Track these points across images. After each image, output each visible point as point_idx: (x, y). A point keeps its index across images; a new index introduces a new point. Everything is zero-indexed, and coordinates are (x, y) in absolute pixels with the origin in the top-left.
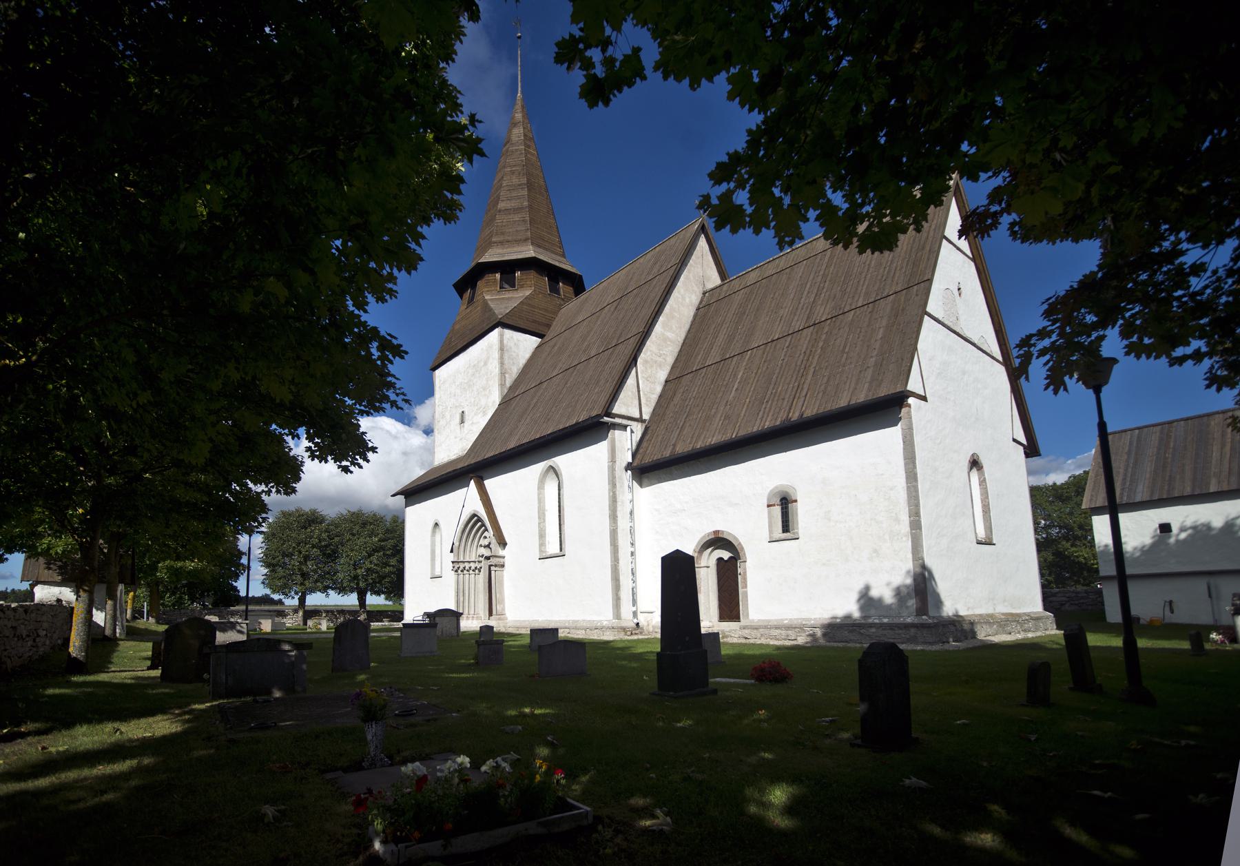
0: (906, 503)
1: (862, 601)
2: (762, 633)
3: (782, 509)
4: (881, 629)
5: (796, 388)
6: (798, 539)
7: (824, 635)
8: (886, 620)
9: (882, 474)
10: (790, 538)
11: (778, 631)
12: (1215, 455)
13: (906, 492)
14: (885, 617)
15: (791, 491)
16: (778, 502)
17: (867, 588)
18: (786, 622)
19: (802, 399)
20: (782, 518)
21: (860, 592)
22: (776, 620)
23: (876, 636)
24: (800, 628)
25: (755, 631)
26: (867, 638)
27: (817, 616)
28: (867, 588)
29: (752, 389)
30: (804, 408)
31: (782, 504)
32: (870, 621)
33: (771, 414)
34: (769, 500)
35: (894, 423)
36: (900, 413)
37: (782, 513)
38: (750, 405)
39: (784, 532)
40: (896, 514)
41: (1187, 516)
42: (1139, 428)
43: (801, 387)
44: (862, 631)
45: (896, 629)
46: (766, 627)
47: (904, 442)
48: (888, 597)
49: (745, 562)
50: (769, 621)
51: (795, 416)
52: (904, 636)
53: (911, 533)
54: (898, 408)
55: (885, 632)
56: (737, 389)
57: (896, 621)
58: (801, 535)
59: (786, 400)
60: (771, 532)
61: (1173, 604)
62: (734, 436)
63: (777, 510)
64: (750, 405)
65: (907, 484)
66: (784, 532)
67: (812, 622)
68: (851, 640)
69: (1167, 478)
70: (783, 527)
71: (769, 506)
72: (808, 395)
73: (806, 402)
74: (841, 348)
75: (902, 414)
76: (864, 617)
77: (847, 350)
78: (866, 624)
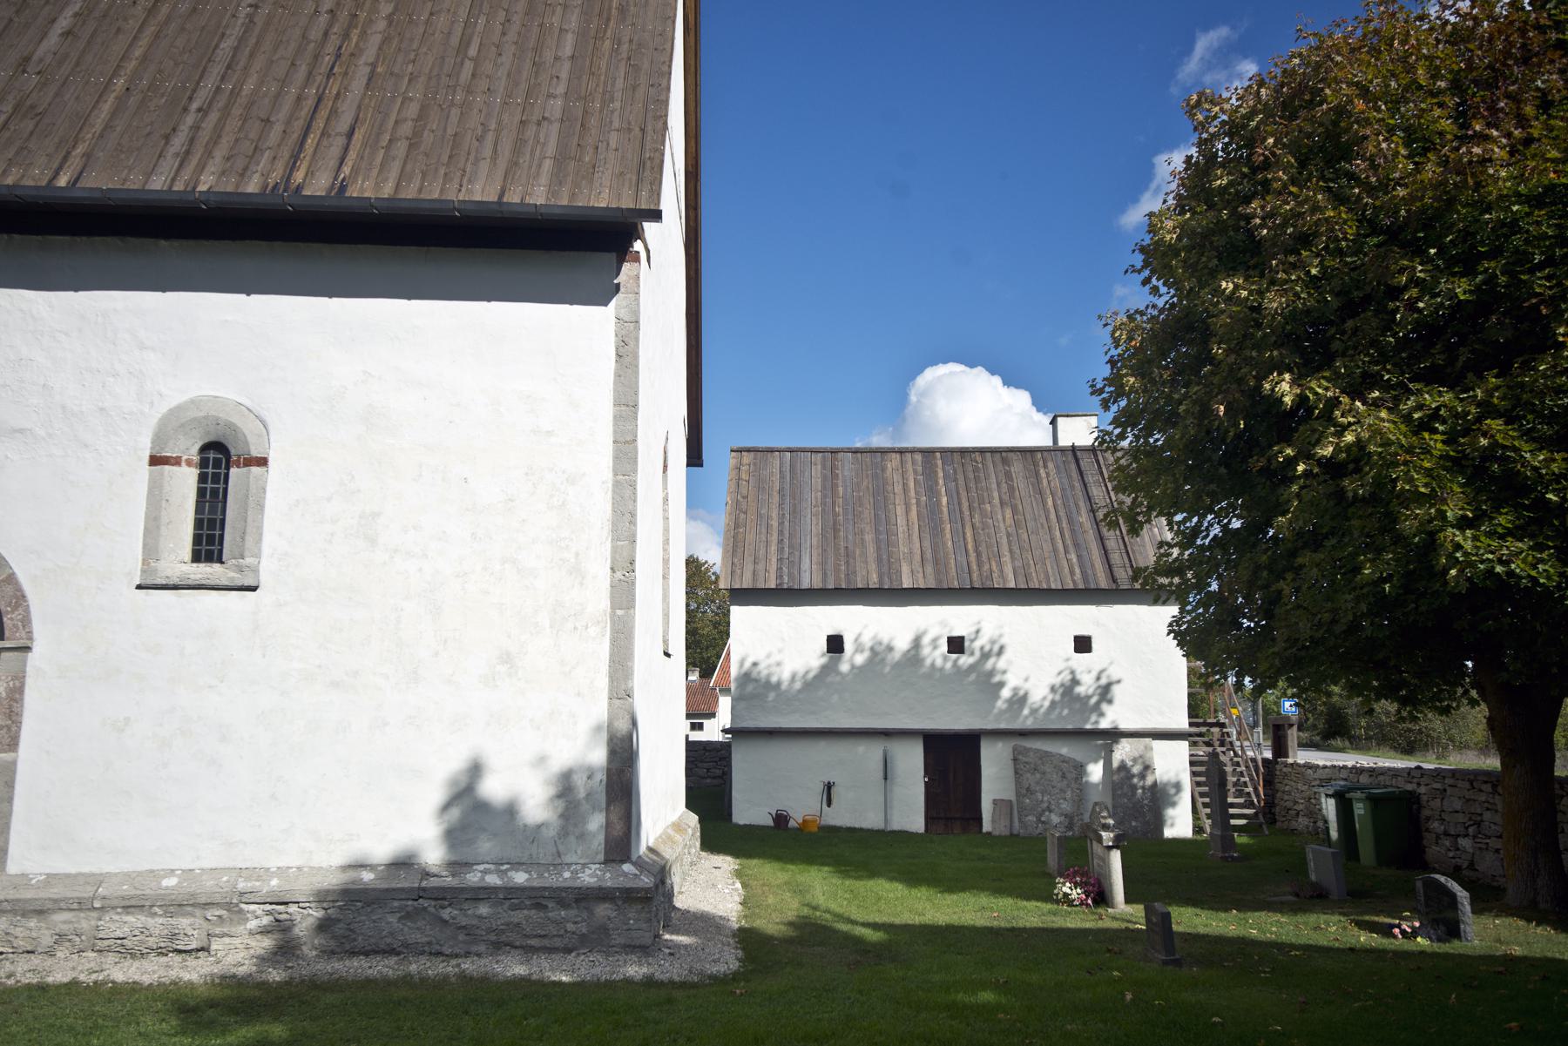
0: (608, 527)
1: (455, 813)
2: (65, 927)
3: (202, 478)
4: (507, 903)
5: (309, 104)
6: (254, 589)
7: (323, 926)
8: (520, 878)
9: (549, 433)
10: (225, 582)
11: (135, 920)
12: (901, 521)
13: (610, 494)
14: (517, 865)
15: (249, 428)
16: (193, 453)
17: (475, 770)
18: (170, 882)
19: (340, 142)
20: (199, 509)
21: (453, 782)
22: (128, 876)
23: (490, 931)
24: (229, 906)
25: (32, 923)
26: (461, 937)
27: (291, 860)
28: (475, 770)
29: (138, 53)
30: (346, 170)
31: (203, 463)
32: (473, 878)
33: (219, 154)
34: (159, 437)
35: (602, 294)
36: (618, 274)
37: (201, 493)
38: (133, 101)
39: (197, 558)
40: (577, 555)
41: (866, 626)
42: (791, 451)
43: (328, 104)
44: (446, 914)
45: (551, 905)
46: (83, 905)
47: (619, 356)
48: (536, 805)
49: (27, 649)
50: (98, 879)
51: (317, 185)
52: (570, 927)
53: (613, 614)
54: (613, 256)
55: (518, 916)
56: (67, 34)
57: (551, 880)
58: (265, 579)
59: (277, 129)
60: (151, 551)
61: (834, 790)
62: (62, 181)
63: (185, 482)
64: (133, 101)
65: (615, 474)
66: (197, 558)
67: (274, 882)
68: (406, 945)
69: (842, 551)
70: (197, 540)
71: (155, 461)
72: (358, 136)
73: (352, 155)
74: (455, 40)
75: (621, 279)
76: (457, 866)
77: (472, 52)
78: (462, 890)
